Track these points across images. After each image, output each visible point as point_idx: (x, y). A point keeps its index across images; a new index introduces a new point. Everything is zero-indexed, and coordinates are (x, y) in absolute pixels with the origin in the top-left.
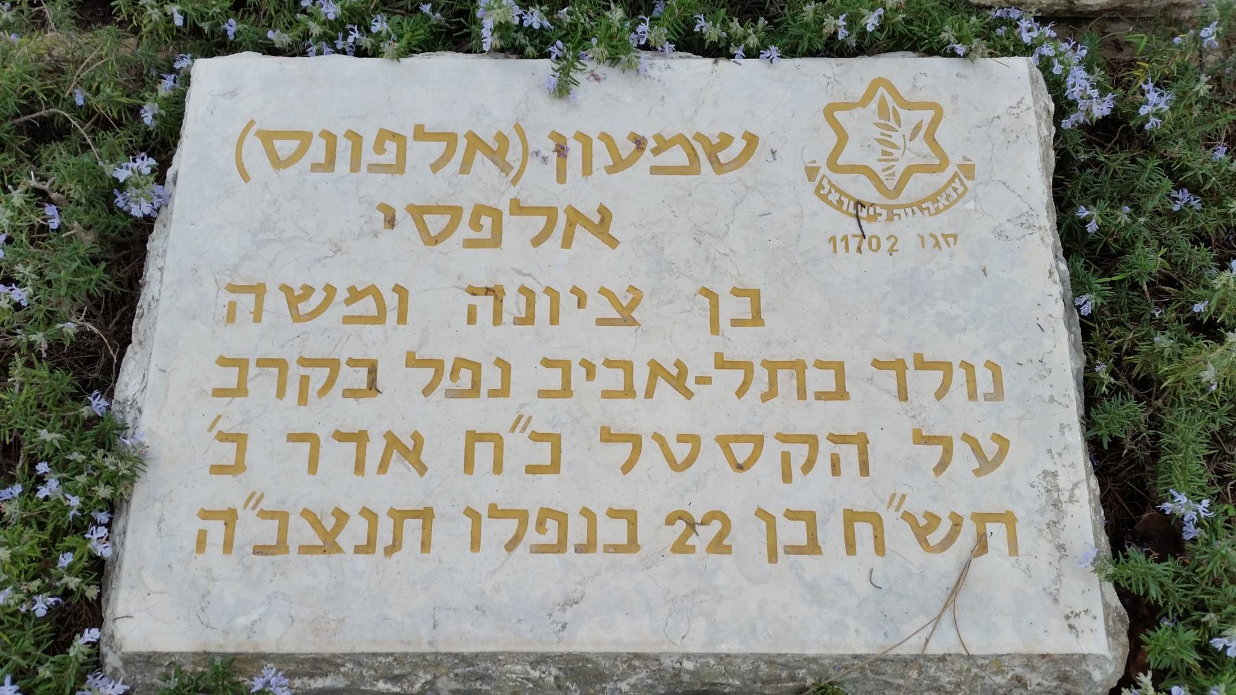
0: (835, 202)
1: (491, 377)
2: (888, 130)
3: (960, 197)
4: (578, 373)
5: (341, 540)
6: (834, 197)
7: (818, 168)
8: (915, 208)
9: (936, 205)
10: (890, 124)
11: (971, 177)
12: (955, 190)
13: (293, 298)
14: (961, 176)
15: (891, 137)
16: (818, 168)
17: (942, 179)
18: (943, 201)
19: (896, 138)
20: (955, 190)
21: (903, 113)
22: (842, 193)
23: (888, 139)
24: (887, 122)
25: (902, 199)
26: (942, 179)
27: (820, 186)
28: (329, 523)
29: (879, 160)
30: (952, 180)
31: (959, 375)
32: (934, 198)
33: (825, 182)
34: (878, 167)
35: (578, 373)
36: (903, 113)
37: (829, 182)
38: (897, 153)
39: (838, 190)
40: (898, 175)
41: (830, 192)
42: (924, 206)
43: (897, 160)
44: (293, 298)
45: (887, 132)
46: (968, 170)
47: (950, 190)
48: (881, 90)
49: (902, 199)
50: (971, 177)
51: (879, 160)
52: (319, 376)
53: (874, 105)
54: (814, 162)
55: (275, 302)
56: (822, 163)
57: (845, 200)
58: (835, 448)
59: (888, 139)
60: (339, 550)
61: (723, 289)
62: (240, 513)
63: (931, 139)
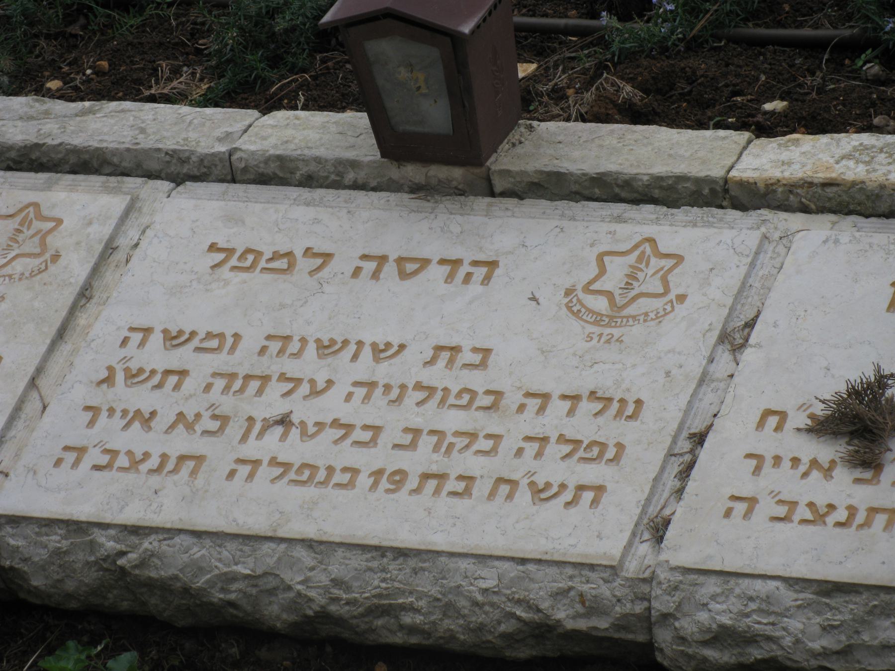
19: (640, 275)
22: (583, 306)
27: (571, 301)
38: (635, 284)
53: (637, 253)
56: (579, 287)
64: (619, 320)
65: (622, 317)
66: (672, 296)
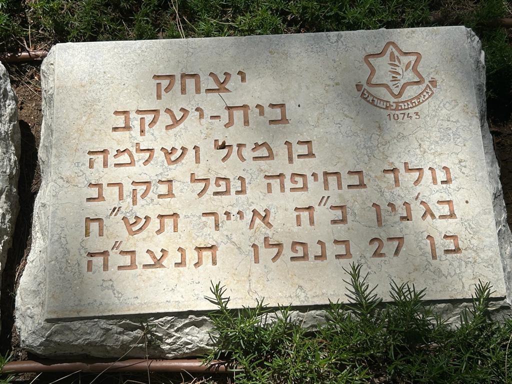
0: (371, 101)
1: (236, 185)
2: (396, 74)
3: (430, 96)
4: (310, 179)
5: (165, 262)
6: (370, 99)
7: (362, 85)
8: (409, 103)
9: (418, 101)
10: (395, 63)
11: (435, 86)
12: (427, 93)
13: (168, 153)
14: (431, 87)
15: (396, 69)
16: (362, 85)
17: (423, 86)
18: (422, 99)
19: (399, 70)
20: (427, 93)
21: (401, 58)
22: (374, 97)
23: (393, 67)
24: (393, 63)
25: (403, 99)
26: (423, 86)
27: (363, 94)
28: (159, 255)
29: (391, 81)
30: (426, 89)
31: (427, 173)
32: (418, 97)
33: (365, 92)
34: (390, 84)
35: (310, 179)
36: (401, 58)
37: (367, 92)
38: (399, 77)
39: (372, 95)
40: (400, 87)
41: (368, 96)
42: (413, 101)
43: (399, 80)
44: (168, 153)
45: (395, 68)
46: (433, 82)
47: (425, 94)
48: (391, 47)
49: (400, 100)
50: (435, 86)
51: (391, 81)
52: (141, 189)
54: (360, 82)
55: (159, 156)
57: (376, 100)
58: (402, 169)
59: (393, 67)
60: (162, 266)
61: (294, 141)
62: (111, 253)
63: (415, 69)
64: (402, 104)
65: (402, 102)
66: (427, 82)
